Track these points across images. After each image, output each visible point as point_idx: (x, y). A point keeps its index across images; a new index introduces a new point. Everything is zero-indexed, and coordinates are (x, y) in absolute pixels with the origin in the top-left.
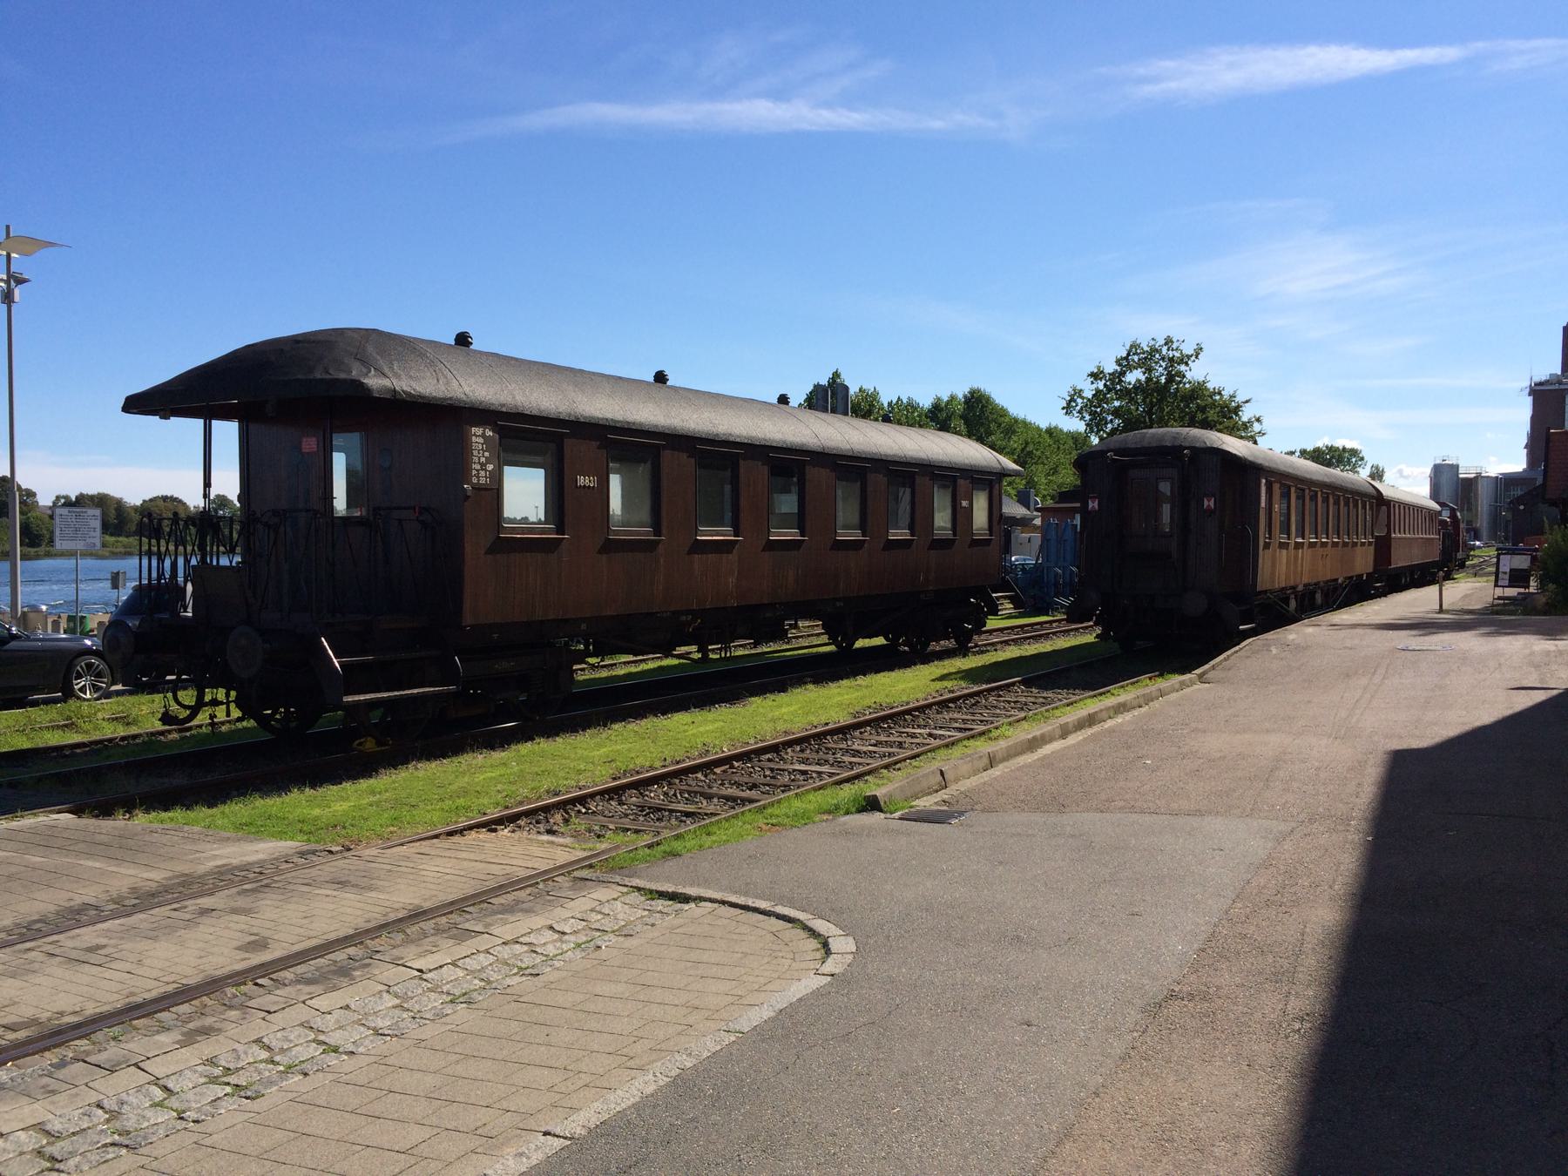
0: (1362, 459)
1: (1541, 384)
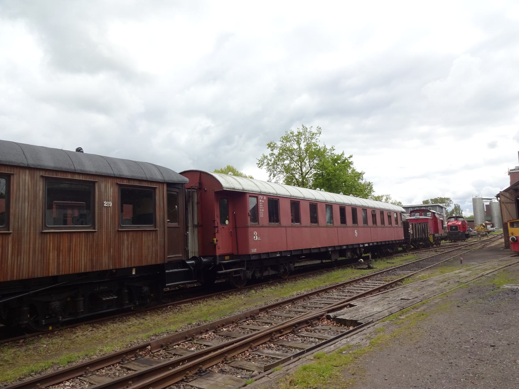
0: (451, 201)
1: (511, 170)
